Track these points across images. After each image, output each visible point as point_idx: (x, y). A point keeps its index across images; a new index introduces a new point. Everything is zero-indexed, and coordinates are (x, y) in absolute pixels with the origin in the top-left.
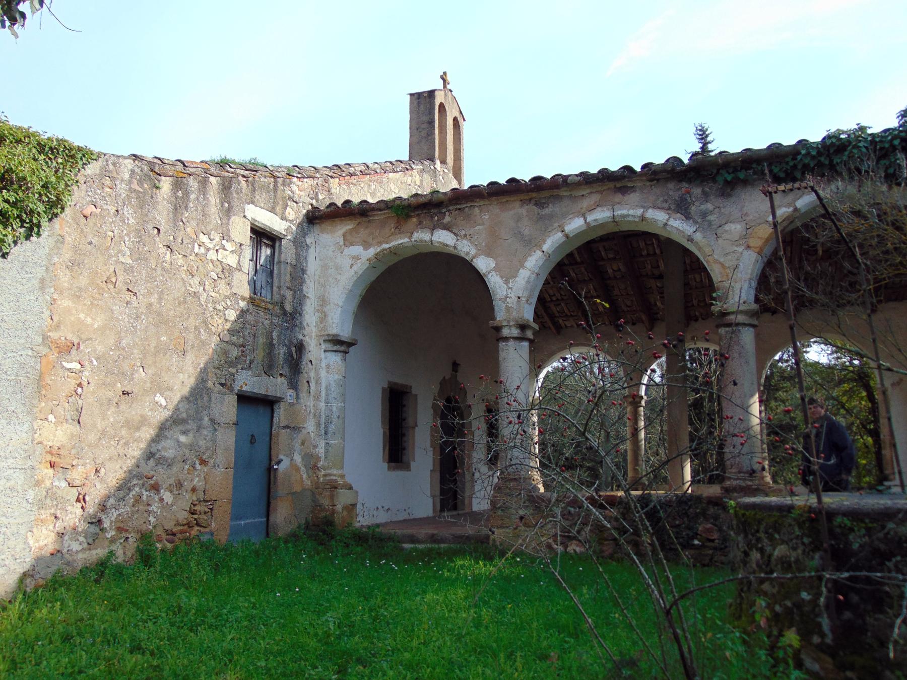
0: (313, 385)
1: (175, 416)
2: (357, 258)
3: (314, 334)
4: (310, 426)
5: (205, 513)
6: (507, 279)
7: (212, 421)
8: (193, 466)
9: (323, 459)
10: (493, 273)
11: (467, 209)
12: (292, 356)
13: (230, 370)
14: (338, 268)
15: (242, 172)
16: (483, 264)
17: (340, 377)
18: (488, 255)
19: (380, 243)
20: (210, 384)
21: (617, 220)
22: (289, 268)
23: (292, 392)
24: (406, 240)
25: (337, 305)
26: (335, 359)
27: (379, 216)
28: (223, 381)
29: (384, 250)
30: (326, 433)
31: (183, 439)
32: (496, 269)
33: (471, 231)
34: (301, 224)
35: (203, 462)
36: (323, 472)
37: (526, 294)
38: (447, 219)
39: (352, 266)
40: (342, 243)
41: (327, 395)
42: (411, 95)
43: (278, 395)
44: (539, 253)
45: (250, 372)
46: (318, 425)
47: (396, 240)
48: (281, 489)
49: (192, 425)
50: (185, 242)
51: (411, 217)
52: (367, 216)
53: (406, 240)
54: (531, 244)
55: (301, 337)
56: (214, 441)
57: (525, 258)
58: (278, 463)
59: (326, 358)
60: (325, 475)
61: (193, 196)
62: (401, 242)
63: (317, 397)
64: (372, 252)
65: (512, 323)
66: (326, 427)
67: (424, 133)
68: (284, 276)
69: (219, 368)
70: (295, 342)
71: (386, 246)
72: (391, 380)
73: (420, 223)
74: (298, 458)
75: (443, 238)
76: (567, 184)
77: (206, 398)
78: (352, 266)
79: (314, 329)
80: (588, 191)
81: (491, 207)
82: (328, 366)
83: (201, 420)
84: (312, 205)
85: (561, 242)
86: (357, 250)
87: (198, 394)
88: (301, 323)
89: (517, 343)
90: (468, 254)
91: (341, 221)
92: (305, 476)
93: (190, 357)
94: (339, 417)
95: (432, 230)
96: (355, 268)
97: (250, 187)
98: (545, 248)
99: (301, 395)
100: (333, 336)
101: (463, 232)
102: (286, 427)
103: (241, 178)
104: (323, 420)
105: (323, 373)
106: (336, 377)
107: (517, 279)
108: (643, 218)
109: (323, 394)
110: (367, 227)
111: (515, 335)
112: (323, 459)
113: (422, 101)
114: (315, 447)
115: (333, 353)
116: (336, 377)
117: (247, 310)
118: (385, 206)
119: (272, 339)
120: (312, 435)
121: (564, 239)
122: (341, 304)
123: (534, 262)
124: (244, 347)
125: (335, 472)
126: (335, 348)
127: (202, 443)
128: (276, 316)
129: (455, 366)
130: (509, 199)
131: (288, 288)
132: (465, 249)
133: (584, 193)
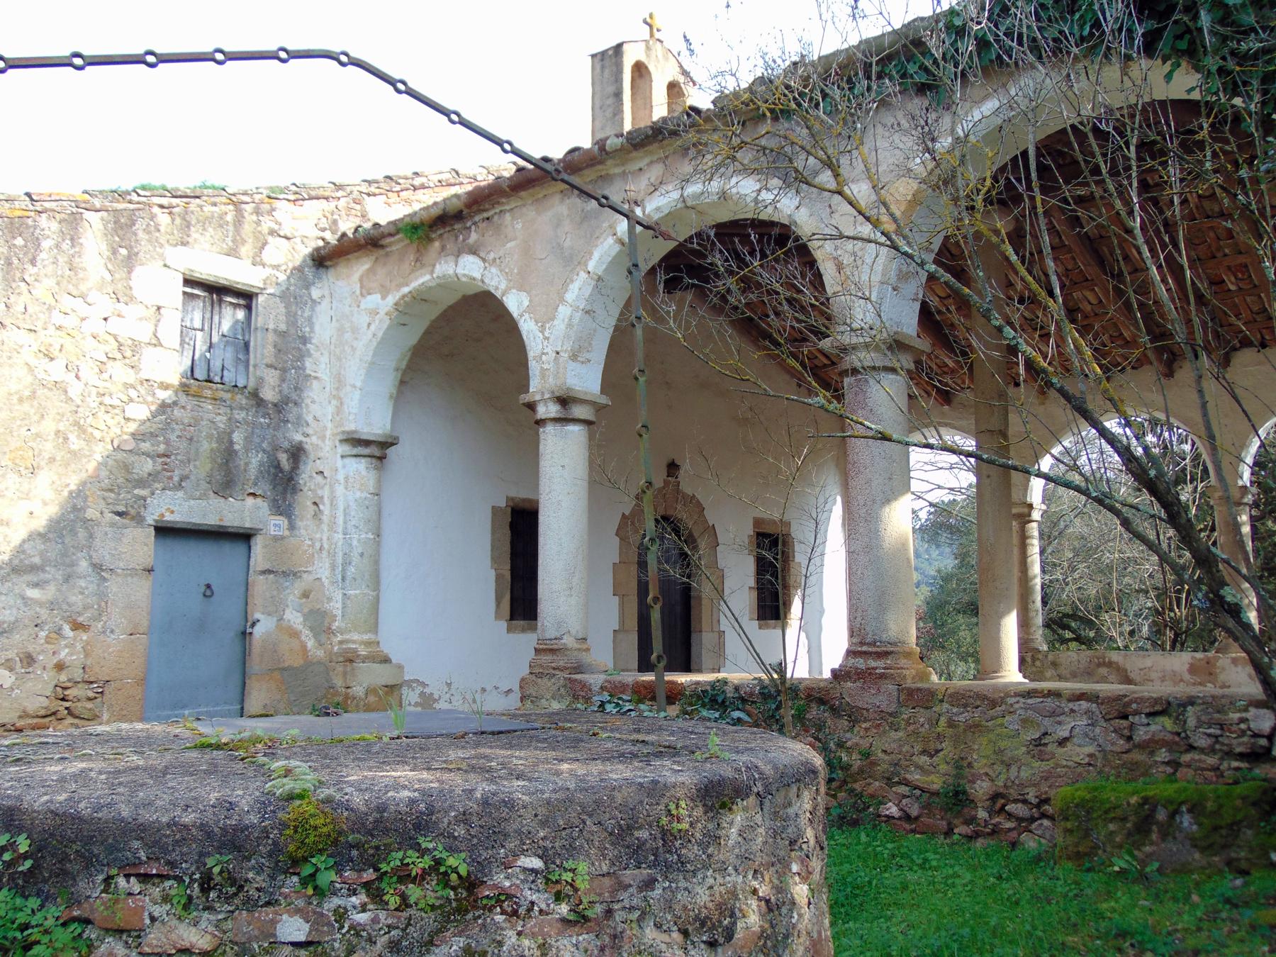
0: (326, 508)
1: (16, 562)
2: (374, 312)
3: (328, 433)
4: (322, 570)
5: (90, 699)
6: (544, 322)
7: (98, 567)
8: (59, 632)
9: (339, 618)
10: (527, 316)
11: (496, 218)
12: (278, 466)
13: (136, 492)
14: (355, 330)
15: (165, 201)
16: (514, 303)
17: (365, 495)
18: (521, 288)
19: (399, 286)
20: (91, 513)
21: (689, 203)
22: (271, 337)
23: (282, 521)
24: (428, 277)
25: (354, 386)
26: (359, 468)
27: (397, 244)
28: (121, 508)
29: (404, 296)
30: (343, 579)
31: (33, 593)
32: (530, 309)
33: (501, 253)
34: (299, 269)
35: (77, 626)
36: (340, 638)
37: (568, 346)
38: (474, 237)
39: (369, 325)
40: (358, 292)
41: (345, 523)
42: (593, 56)
43: (247, 525)
44: (583, 275)
45: (180, 494)
46: (333, 567)
47: (416, 279)
48: (255, 665)
49: (51, 573)
50: (30, 310)
51: (430, 240)
52: (382, 247)
53: (428, 277)
54: (573, 261)
55: (298, 437)
56: (102, 596)
57: (565, 286)
58: (253, 625)
59: (344, 467)
60: (341, 642)
61: (46, 244)
62: (421, 281)
63: (332, 526)
64: (391, 300)
65: (547, 396)
66: (344, 570)
67: (609, 113)
68: (263, 349)
69: (111, 491)
70: (286, 445)
71: (406, 290)
72: (513, 494)
73: (443, 248)
74: (294, 618)
75: (469, 269)
76: (607, 153)
77: (82, 534)
78: (369, 325)
79: (329, 425)
80: (647, 160)
81: (524, 210)
82: (347, 478)
83: (72, 565)
84: (323, 240)
85: (613, 253)
86: (374, 300)
87: (68, 528)
88: (299, 417)
89: (558, 427)
90: (497, 288)
91: (357, 258)
92: (310, 644)
93: (46, 477)
94: (362, 555)
95: (458, 255)
96: (373, 327)
97: (178, 221)
98: (591, 266)
99: (299, 523)
100: (348, 433)
101: (492, 256)
102: (269, 572)
103: (156, 210)
104: (340, 560)
105: (340, 490)
106: (358, 494)
107: (556, 322)
108: (724, 195)
109: (340, 520)
110: (385, 264)
111: (552, 415)
112: (339, 618)
113: (607, 62)
114: (330, 599)
115: (353, 460)
116: (358, 494)
117: (175, 403)
118: (397, 228)
119: (231, 443)
120: (326, 582)
121: (617, 248)
122: (359, 384)
123: (576, 291)
124: (168, 456)
125: (356, 638)
126: (355, 451)
127: (76, 599)
128: (241, 408)
129: (673, 467)
130: (545, 192)
131: (269, 366)
132: (495, 281)
133: (642, 164)
